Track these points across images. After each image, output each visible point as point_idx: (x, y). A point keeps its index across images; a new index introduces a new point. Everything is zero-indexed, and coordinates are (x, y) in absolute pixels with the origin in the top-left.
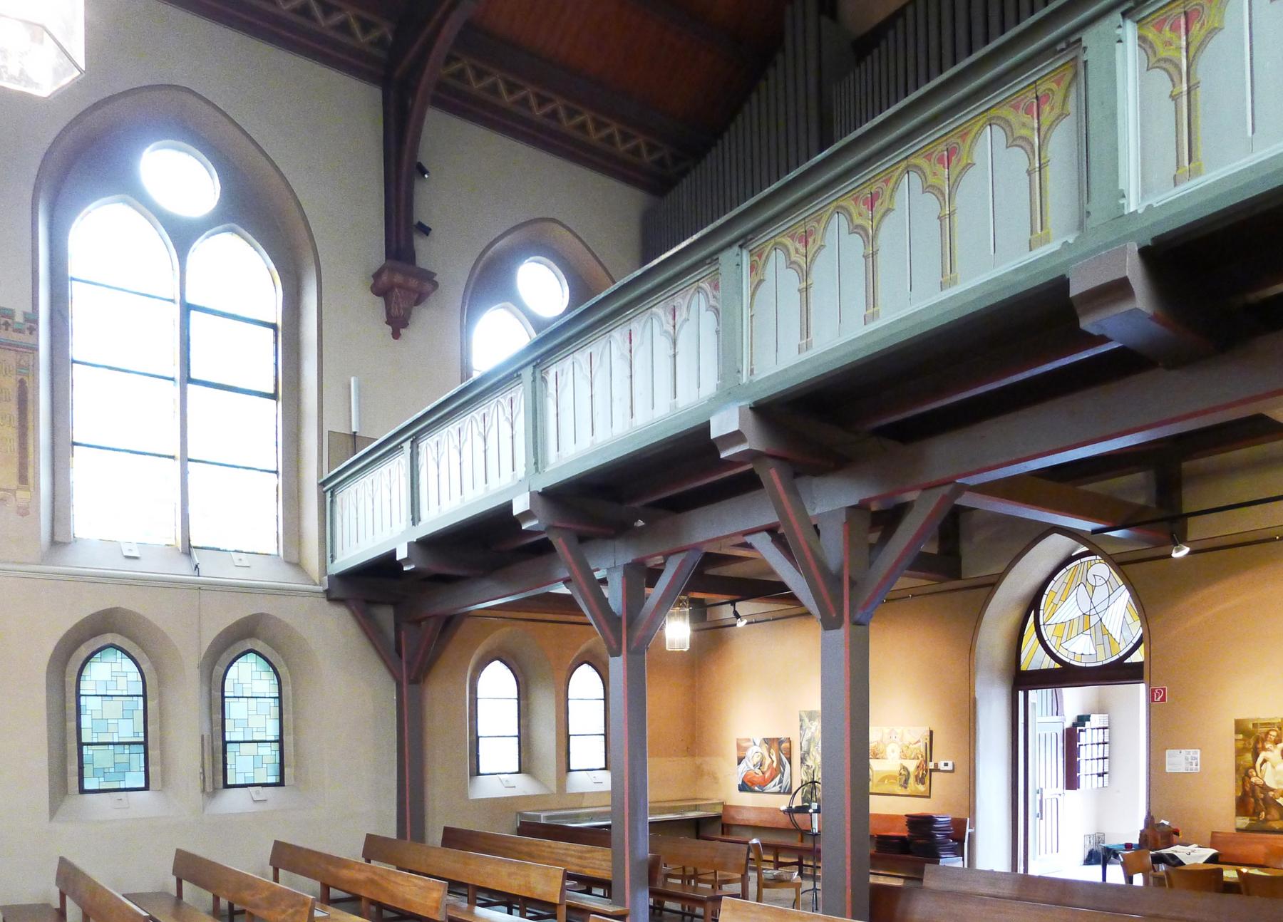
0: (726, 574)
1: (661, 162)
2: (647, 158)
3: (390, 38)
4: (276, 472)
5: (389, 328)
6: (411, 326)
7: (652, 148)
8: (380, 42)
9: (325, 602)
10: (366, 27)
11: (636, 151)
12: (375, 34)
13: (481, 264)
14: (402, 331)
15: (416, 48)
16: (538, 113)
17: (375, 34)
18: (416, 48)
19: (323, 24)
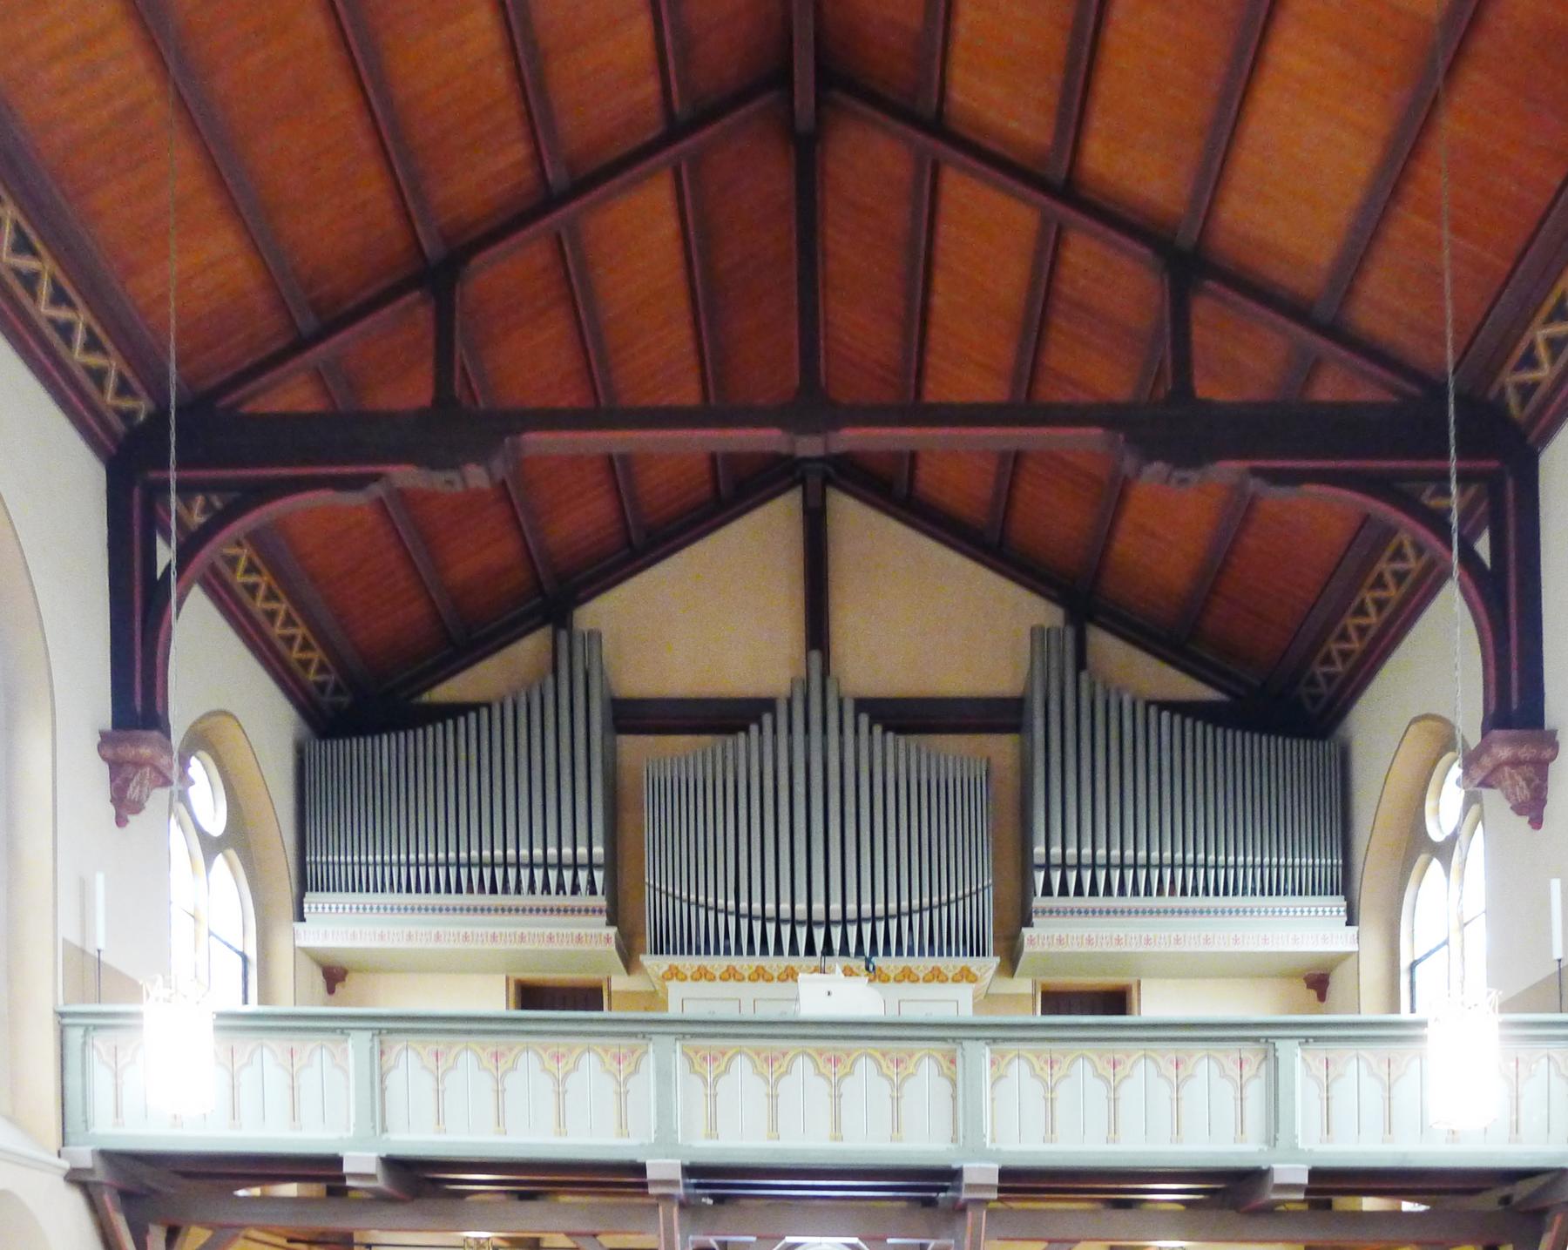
0: (1171, 673)
1: (321, 687)
2: (312, 676)
3: (142, 417)
4: (210, 934)
5: (112, 809)
6: (143, 813)
7: (322, 669)
8: (126, 416)
9: (61, 1183)
10: (123, 389)
11: (305, 664)
12: (127, 404)
13: (1368, 666)
14: (131, 818)
15: (285, 472)
16: (240, 578)
17: (127, 404)
18: (285, 472)
19: (76, 355)
